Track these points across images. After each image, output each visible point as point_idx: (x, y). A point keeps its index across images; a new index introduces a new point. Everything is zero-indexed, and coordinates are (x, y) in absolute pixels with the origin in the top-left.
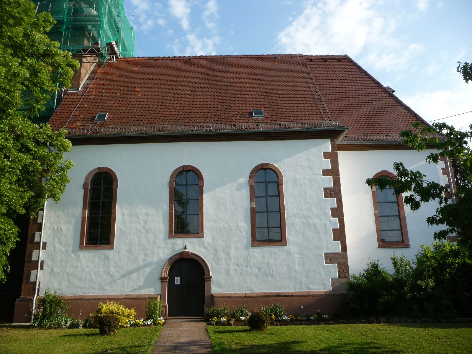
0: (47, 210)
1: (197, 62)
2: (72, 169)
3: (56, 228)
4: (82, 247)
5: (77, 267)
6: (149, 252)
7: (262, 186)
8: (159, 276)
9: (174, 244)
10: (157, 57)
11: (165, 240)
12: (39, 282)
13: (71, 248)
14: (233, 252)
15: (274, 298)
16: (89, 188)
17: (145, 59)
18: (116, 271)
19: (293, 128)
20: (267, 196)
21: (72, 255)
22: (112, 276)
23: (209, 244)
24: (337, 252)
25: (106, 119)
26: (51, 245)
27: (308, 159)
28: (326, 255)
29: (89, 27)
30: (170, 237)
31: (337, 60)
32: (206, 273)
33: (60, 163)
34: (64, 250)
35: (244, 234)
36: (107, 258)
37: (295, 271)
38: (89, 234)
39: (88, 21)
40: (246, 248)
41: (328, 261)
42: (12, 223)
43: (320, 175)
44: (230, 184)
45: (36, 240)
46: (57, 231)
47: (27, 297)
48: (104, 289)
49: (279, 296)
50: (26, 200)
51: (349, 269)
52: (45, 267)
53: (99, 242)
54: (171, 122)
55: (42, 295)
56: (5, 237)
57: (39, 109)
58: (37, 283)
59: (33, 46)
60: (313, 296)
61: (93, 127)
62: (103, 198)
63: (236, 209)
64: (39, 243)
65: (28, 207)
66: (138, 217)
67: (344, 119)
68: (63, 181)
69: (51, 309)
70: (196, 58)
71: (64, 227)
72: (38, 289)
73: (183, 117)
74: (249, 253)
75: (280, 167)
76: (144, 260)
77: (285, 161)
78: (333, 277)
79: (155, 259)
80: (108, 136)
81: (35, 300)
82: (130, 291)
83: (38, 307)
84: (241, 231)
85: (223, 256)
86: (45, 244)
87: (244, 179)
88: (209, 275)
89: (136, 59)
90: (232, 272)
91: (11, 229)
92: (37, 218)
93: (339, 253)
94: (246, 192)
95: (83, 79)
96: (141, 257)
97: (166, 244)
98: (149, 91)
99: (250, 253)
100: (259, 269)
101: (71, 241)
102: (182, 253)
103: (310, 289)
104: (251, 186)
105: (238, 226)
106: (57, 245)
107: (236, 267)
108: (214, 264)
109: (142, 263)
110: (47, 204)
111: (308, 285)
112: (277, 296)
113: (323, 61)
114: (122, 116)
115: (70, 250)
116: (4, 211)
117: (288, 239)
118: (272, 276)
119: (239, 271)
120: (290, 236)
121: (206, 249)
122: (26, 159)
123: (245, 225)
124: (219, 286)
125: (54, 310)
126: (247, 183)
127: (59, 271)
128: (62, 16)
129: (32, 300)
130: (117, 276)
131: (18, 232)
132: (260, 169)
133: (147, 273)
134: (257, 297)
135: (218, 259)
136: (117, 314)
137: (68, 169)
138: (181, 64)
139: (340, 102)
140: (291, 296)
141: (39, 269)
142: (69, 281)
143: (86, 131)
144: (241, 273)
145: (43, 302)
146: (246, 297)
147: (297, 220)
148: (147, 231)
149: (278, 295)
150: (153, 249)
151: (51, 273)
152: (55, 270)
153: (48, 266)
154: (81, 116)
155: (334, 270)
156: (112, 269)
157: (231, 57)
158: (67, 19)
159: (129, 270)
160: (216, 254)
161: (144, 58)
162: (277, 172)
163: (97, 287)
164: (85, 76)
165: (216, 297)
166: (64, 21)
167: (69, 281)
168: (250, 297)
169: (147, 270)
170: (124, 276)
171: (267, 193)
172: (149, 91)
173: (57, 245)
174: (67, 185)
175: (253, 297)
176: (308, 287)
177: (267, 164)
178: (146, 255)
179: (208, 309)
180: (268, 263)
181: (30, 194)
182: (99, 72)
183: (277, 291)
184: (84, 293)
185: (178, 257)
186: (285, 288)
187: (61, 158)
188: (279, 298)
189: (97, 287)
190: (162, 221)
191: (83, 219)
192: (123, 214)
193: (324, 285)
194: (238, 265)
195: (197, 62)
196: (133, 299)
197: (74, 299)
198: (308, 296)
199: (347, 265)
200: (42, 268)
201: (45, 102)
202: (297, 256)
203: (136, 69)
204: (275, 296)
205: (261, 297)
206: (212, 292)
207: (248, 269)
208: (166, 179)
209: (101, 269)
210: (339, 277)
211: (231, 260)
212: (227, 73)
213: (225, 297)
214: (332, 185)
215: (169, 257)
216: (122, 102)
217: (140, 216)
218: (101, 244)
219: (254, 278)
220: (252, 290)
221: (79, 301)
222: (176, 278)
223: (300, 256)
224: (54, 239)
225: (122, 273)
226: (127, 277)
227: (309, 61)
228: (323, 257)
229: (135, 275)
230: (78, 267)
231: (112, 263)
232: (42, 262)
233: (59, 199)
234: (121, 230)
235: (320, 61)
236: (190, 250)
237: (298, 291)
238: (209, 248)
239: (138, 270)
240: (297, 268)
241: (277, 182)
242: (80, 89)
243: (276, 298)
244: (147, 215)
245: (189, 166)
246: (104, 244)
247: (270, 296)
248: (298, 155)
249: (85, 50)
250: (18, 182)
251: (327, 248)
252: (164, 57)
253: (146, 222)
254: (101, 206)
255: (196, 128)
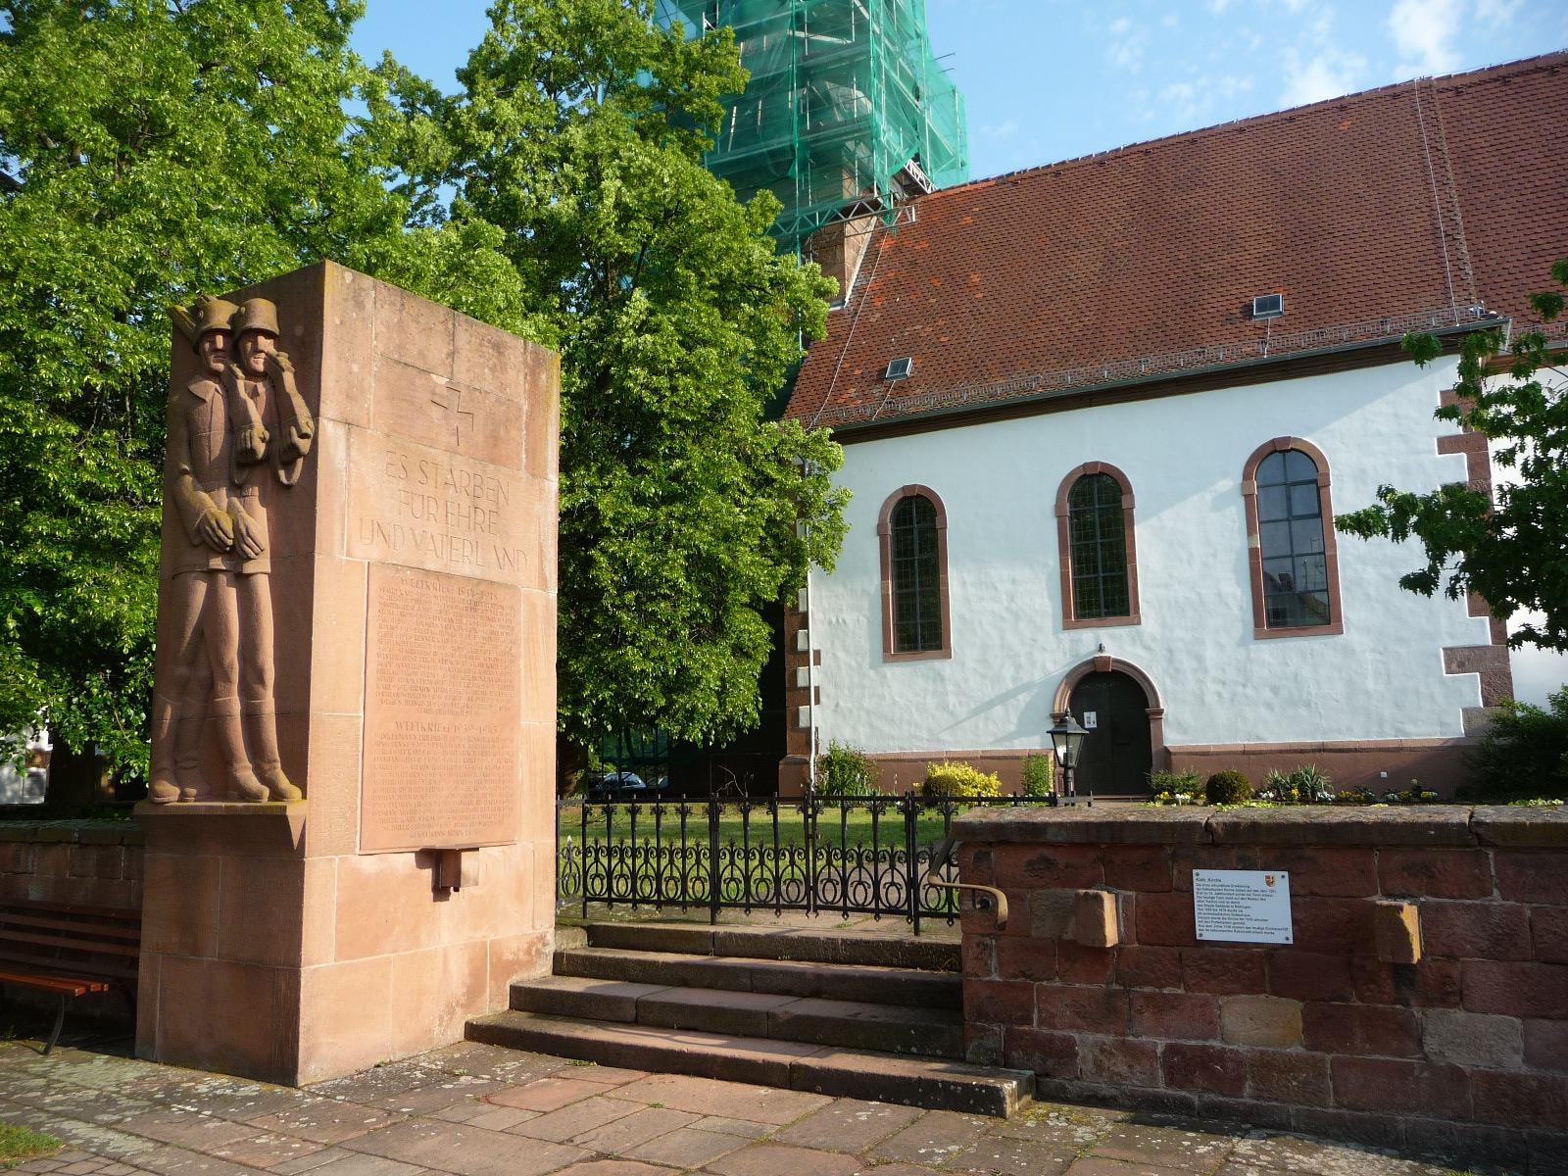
0: (814, 584)
1: (1120, 169)
2: (850, 503)
3: (834, 620)
4: (887, 657)
5: (883, 697)
6: (1023, 660)
7: (1278, 493)
8: (1047, 713)
9: (1075, 642)
10: (1019, 173)
11: (1055, 633)
12: (817, 729)
13: (868, 660)
14: (1210, 654)
15: (1311, 755)
16: (890, 533)
17: (989, 184)
18: (960, 702)
19: (1351, 339)
20: (1290, 518)
21: (872, 673)
22: (952, 713)
23: (1154, 639)
24: (1481, 643)
25: (908, 372)
26: (830, 655)
27: (1396, 415)
28: (1450, 652)
29: (850, 145)
30: (1067, 626)
31: (1546, 73)
32: (1151, 703)
33: (825, 496)
34: (853, 663)
35: (1236, 611)
36: (940, 677)
37: (1367, 693)
38: (900, 629)
39: (846, 134)
40: (1242, 643)
41: (1454, 666)
42: (759, 619)
43: (1432, 452)
44: (1195, 497)
45: (801, 646)
46: (837, 626)
47: (799, 756)
48: (939, 740)
49: (1324, 750)
50: (780, 581)
51: (1511, 683)
52: (823, 699)
53: (920, 645)
54: (1052, 361)
55: (824, 752)
56: (750, 644)
57: (774, 386)
58: (813, 730)
59: (749, 272)
60: (1411, 750)
61: (883, 397)
62: (920, 552)
63: (1214, 556)
64: (807, 652)
65: (782, 590)
66: (995, 588)
67: (1540, 272)
68: (837, 530)
69: (842, 776)
70: (1120, 154)
71: (849, 617)
72: (816, 742)
73: (1079, 343)
74: (1249, 654)
75: (1321, 444)
76: (1015, 679)
77: (1336, 426)
78: (1467, 706)
79: (1038, 676)
80: (915, 417)
81: (812, 762)
82: (991, 744)
83: (820, 769)
84: (1227, 604)
85: (1187, 663)
86: (817, 653)
87: (1230, 482)
88: (1158, 705)
89: (969, 188)
90: (1210, 698)
91: (759, 631)
92: (797, 605)
93: (1488, 647)
94: (1236, 512)
95: (851, 274)
96: (1008, 672)
97: (1059, 641)
98: (1000, 279)
99: (1252, 655)
100: (1275, 690)
101: (866, 645)
102: (1093, 661)
103: (1405, 733)
104: (1248, 497)
105: (1219, 595)
106: (841, 654)
107: (1220, 688)
108: (1168, 681)
109: (1011, 686)
110: (813, 572)
111: (1400, 725)
112: (1319, 751)
113: (1497, 83)
114: (942, 361)
115: (866, 663)
116: (745, 599)
117: (1346, 618)
118: (1308, 705)
119: (1226, 695)
120: (1350, 608)
121: (1148, 648)
122: (768, 505)
123: (1238, 592)
124: (1183, 729)
125: (849, 776)
126: (1238, 491)
127: (849, 705)
128: (788, 138)
129: (808, 763)
130: (962, 712)
131: (769, 634)
132: (1272, 453)
133: (1022, 705)
134: (1271, 752)
135: (1177, 670)
136: (963, 782)
137: (842, 505)
138: (1080, 183)
139: (1536, 218)
140: (1356, 750)
141: (813, 702)
142: (871, 726)
143: (869, 411)
144: (1232, 700)
145: (827, 763)
146: (1244, 753)
147: (1370, 569)
148: (1017, 617)
149: (1322, 749)
150: (1031, 654)
151: (835, 711)
152: (841, 703)
153: (828, 696)
154: (857, 372)
155: (1470, 689)
156: (952, 700)
157: (1216, 131)
158: (799, 142)
159: (987, 699)
160: (1170, 661)
161: (987, 180)
162: (1308, 452)
163: (925, 735)
164: (854, 265)
165: (1175, 754)
166: (792, 147)
167: (871, 726)
168: (1254, 753)
169: (1023, 698)
170: (976, 712)
171: (1289, 509)
172: (1000, 279)
173: (841, 654)
174: (845, 536)
175: (1261, 753)
176: (1399, 731)
177: (1287, 440)
178: (1018, 667)
179: (1157, 777)
180: (1296, 675)
181: (785, 569)
182: (884, 245)
183: (1319, 739)
184: (901, 748)
185: (1088, 669)
186: (1339, 731)
187: (827, 487)
188: (1325, 754)
189: (925, 735)
190: (1045, 593)
191: (885, 597)
192: (964, 583)
193: (1442, 724)
194: (1224, 683)
195: (1120, 169)
196: (999, 758)
197: (885, 761)
198: (1399, 750)
199: (1509, 676)
200: (817, 702)
201: (784, 370)
202: (1369, 656)
203: (968, 219)
204: (1314, 751)
205: (1280, 752)
206: (1167, 744)
207: (1249, 691)
208: (1050, 500)
209: (930, 700)
210: (1485, 704)
211: (1206, 671)
212: (1198, 190)
213: (1197, 754)
214: (1464, 477)
215: (1068, 669)
216: (941, 323)
217: (998, 586)
218: (924, 648)
219: (1263, 712)
220: (1258, 738)
221: (894, 764)
222: (1086, 714)
223: (1378, 657)
224: (833, 643)
225: (973, 706)
226: (982, 715)
227: (1450, 94)
228: (1439, 658)
229: (998, 710)
230: (884, 696)
231: (950, 688)
232: (817, 689)
233: (833, 566)
234: (962, 617)
235: (1489, 86)
236: (1111, 652)
237: (1374, 738)
238: (1153, 645)
239: (1003, 698)
240: (1370, 685)
241: (1315, 481)
242: (847, 300)
243: (1318, 755)
244: (1014, 581)
245: (1096, 463)
246: (931, 648)
247: (1302, 751)
248: (1368, 407)
249: (846, 211)
250: (763, 549)
251: (1452, 636)
252: (1037, 169)
253: (1012, 598)
254: (917, 569)
255: (1108, 373)
